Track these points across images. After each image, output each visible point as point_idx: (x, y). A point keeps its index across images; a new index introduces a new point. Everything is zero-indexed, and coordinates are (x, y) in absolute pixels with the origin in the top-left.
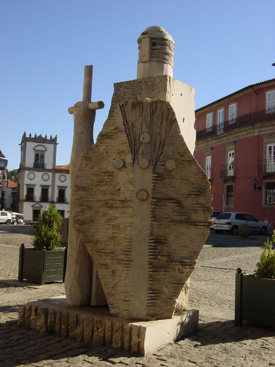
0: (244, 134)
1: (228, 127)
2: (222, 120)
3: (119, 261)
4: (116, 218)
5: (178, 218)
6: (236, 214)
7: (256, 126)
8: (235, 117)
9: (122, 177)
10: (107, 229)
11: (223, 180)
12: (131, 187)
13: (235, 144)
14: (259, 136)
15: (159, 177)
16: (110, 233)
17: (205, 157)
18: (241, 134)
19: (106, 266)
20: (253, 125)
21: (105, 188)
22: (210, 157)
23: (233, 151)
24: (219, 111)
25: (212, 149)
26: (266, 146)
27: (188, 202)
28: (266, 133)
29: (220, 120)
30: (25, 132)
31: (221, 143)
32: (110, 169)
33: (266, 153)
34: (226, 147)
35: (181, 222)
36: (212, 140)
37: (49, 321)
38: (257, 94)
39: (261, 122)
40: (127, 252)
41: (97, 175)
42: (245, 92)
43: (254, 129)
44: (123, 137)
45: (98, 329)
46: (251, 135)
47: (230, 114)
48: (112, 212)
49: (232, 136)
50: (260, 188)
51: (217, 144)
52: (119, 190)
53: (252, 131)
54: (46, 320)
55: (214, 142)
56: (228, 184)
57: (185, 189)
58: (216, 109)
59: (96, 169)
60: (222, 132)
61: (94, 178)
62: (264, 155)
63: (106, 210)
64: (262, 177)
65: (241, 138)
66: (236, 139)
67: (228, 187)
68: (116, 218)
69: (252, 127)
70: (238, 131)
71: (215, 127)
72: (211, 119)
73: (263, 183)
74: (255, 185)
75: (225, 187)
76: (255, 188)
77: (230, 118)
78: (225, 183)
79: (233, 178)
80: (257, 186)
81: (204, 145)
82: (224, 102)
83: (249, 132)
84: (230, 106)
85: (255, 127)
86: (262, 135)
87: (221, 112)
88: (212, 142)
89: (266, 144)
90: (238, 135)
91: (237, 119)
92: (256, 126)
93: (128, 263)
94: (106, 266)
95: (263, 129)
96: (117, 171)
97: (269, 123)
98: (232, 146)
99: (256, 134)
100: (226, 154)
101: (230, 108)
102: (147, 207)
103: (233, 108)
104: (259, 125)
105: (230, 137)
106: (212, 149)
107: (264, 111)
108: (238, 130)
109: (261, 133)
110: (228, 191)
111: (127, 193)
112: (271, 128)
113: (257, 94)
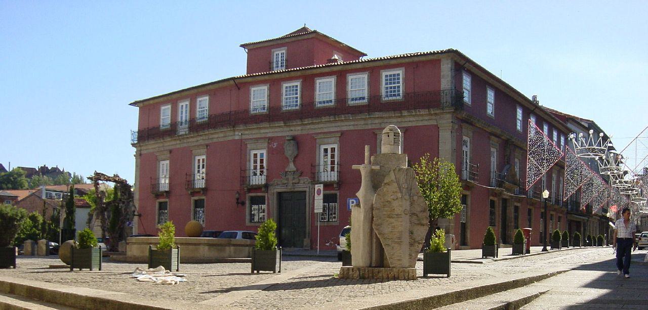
0: (220, 135)
1: (195, 127)
2: (186, 116)
3: (396, 243)
4: (393, 223)
5: (416, 222)
6: (243, 233)
7: (238, 128)
8: (206, 114)
9: (395, 204)
10: (389, 228)
11: (189, 192)
12: (401, 209)
13: (207, 148)
14: (241, 140)
15: (411, 204)
16: (390, 230)
17: (159, 161)
18: (216, 136)
19: (388, 245)
20: (234, 127)
21: (386, 209)
22: (168, 162)
23: (204, 157)
24: (181, 104)
25: (171, 152)
26: (250, 153)
27: (420, 215)
28: (251, 137)
29: (184, 115)
30: (130, 104)
31: (185, 145)
32: (389, 200)
33: (250, 161)
34: (193, 151)
35: (418, 224)
36: (172, 140)
37: (361, 273)
38: (239, 89)
39: (246, 123)
40: (399, 238)
41: (383, 202)
42: (221, 85)
43: (234, 132)
44: (395, 185)
45: (390, 273)
46: (230, 138)
47: (198, 110)
48: (392, 220)
49: (202, 138)
50: (243, 204)
51: (178, 146)
52: (394, 209)
53: (232, 133)
54: (360, 273)
55: (174, 143)
56: (196, 198)
57: (419, 209)
58: (177, 100)
59: (382, 200)
60: (187, 133)
61: (382, 204)
62: (248, 163)
63: (388, 219)
64: (246, 190)
65: (215, 140)
66: (207, 142)
67: (160, 203)
68: (393, 223)
69: (232, 129)
70: (212, 132)
71: (174, 125)
72: (169, 113)
73: (247, 197)
74: (238, 199)
75: (192, 202)
76: (238, 203)
77: (198, 115)
78: (193, 196)
79: (205, 190)
80: (239, 201)
81: (157, 146)
82: (192, 93)
83: (228, 134)
84: (199, 99)
85: (236, 129)
86: (245, 139)
87: (184, 105)
88: (171, 143)
89: (250, 150)
90: (211, 136)
91: (210, 117)
92: (238, 128)
93: (400, 243)
94: (388, 245)
95: (247, 132)
96: (393, 201)
97: (255, 126)
98: (202, 150)
99: (237, 138)
100: (193, 160)
101: (198, 102)
102: (408, 217)
103: (204, 102)
104: (242, 127)
105: (199, 138)
106: (171, 152)
107: (247, 111)
108: (211, 131)
109: (244, 137)
110: (160, 208)
111: (398, 210)
112: (257, 131)
113: (239, 89)
